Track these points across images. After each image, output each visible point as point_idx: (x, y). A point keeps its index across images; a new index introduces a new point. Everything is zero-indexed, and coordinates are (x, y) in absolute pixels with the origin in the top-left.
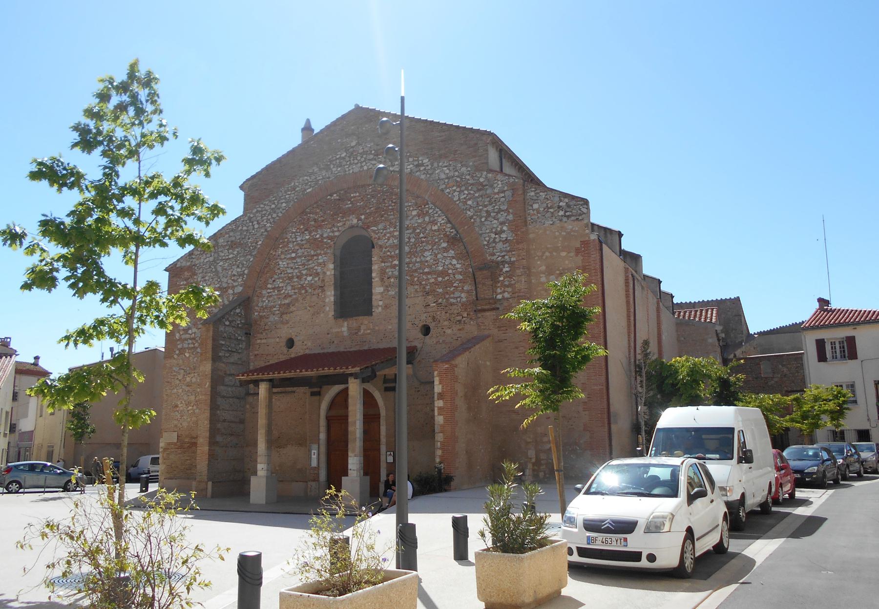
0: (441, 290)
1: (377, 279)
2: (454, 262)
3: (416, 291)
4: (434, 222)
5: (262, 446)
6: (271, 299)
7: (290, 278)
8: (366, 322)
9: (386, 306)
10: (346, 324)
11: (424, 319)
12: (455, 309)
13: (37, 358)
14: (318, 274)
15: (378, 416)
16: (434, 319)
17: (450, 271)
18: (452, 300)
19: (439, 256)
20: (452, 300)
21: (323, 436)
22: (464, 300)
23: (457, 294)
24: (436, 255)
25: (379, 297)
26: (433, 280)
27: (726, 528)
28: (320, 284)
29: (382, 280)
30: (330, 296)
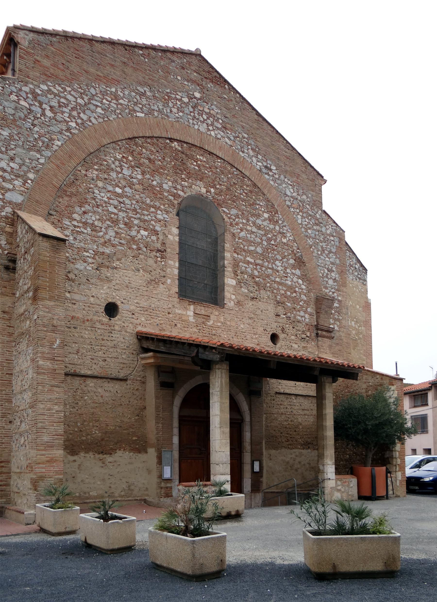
0: (289, 304)
1: (230, 269)
2: (300, 281)
3: (268, 297)
4: (283, 235)
5: (264, 444)
6: (80, 237)
7: (115, 222)
8: (217, 313)
9: (238, 302)
10: (192, 307)
11: (274, 328)
12: (301, 327)
13: (110, 319)
14: (156, 233)
15: (242, 420)
16: (283, 330)
17: (297, 289)
18: (299, 318)
19: (288, 271)
20: (299, 318)
21: (176, 440)
22: (307, 320)
23: (302, 313)
24: (286, 268)
25: (231, 290)
26: (283, 292)
27: (230, 563)
28: (158, 246)
29: (235, 273)
30: (173, 266)
